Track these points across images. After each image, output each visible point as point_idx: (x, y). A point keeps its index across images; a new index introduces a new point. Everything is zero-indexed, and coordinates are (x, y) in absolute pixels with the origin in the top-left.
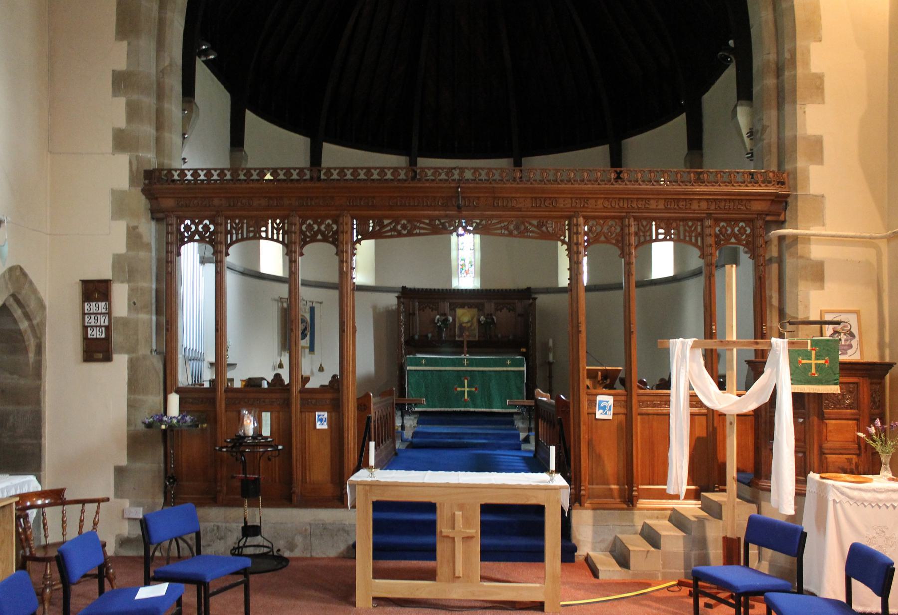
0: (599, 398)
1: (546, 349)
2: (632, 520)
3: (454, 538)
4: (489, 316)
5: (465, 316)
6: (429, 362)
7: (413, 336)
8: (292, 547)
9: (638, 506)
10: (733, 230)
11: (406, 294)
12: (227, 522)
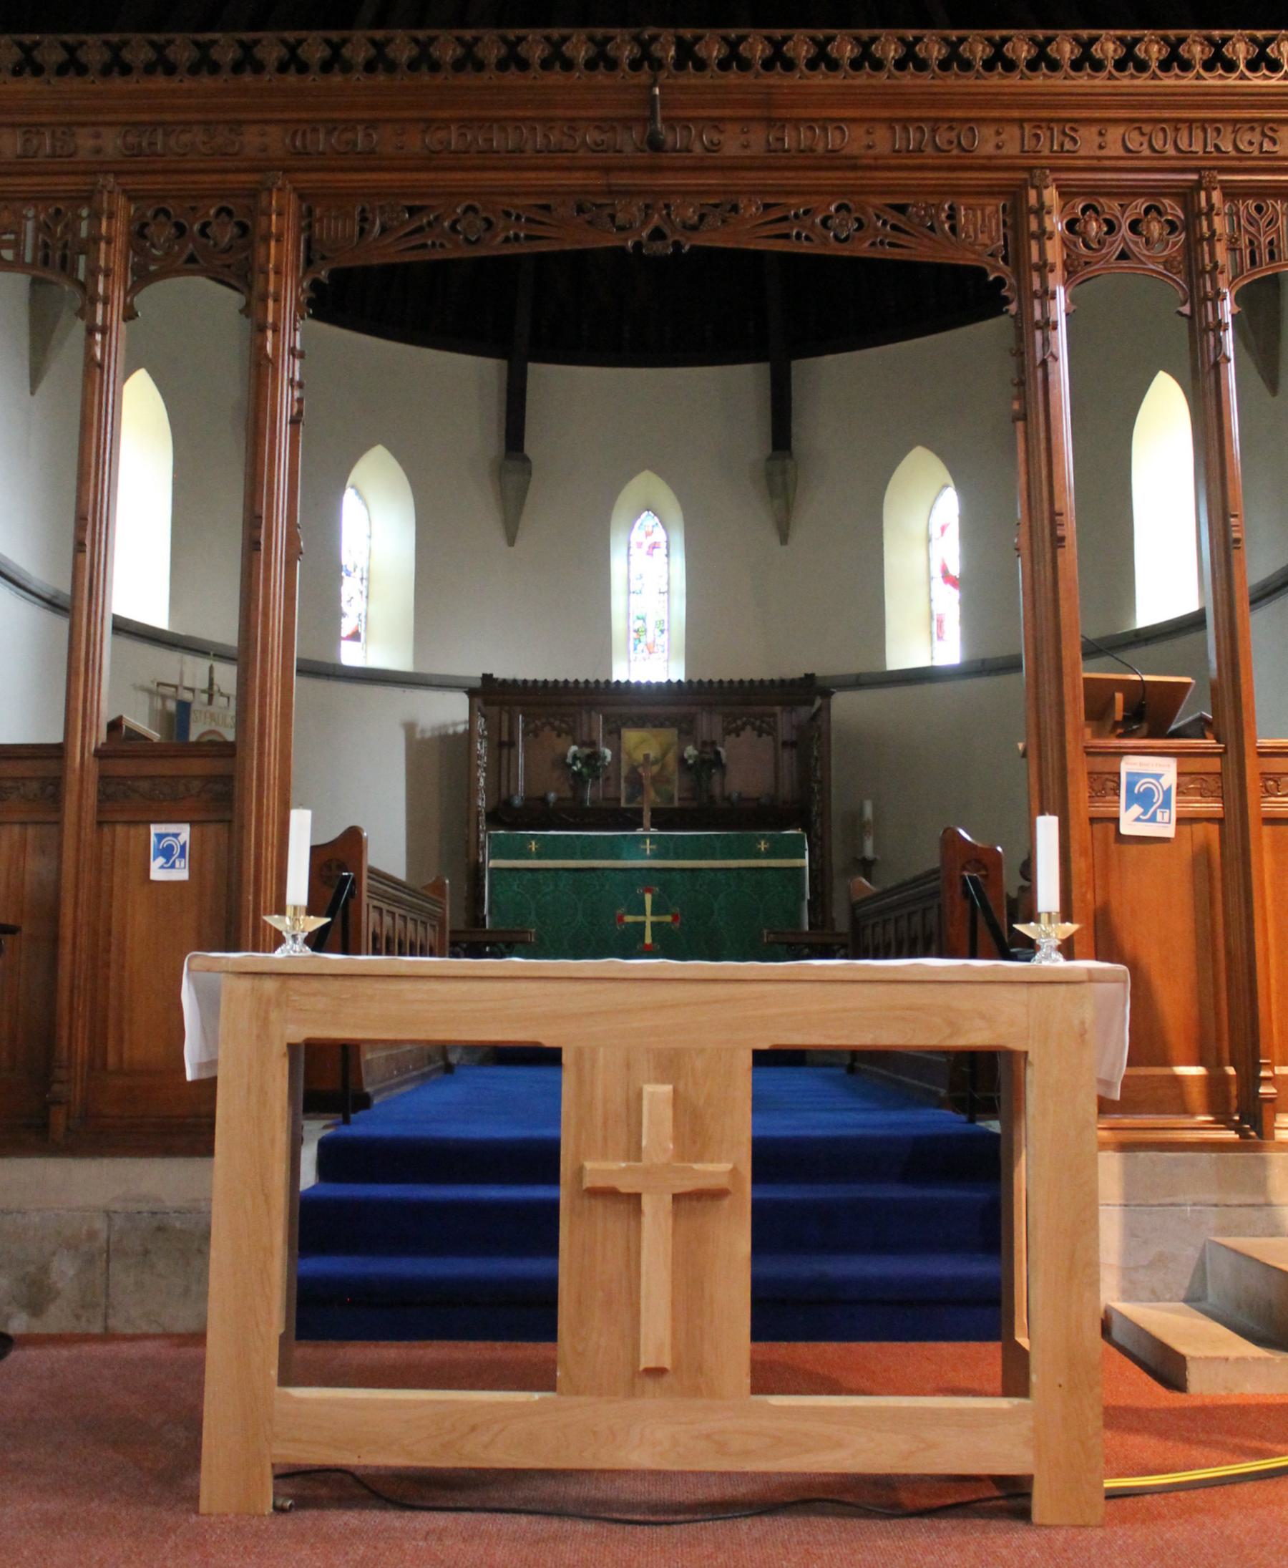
0: (1129, 765)
1: (856, 826)
2: (1261, 1185)
3: (636, 1198)
5: (641, 744)
7: (510, 798)
11: (489, 694)
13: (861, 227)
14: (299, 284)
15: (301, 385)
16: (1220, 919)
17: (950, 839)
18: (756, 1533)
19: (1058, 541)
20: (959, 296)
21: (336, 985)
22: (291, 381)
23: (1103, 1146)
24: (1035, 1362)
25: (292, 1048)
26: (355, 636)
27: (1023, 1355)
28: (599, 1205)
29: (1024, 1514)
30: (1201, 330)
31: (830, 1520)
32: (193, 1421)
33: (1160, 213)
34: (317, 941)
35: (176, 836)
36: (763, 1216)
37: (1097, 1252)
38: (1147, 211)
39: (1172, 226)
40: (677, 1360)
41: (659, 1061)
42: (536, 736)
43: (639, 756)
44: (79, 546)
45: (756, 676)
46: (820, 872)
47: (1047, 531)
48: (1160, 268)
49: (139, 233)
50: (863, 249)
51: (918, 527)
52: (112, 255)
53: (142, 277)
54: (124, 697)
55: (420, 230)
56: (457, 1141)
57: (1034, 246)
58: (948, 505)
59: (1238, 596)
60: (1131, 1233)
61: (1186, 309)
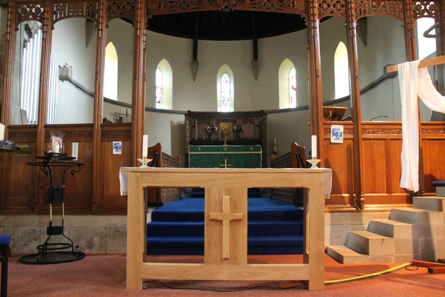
0: (333, 127)
1: (273, 144)
2: (361, 220)
3: (222, 221)
4: (239, 126)
5: (224, 126)
8: (90, 245)
9: (365, 209)
10: (425, 7)
11: (190, 115)
12: (41, 227)
13: (272, 5)
14: (145, 19)
15: (146, 42)
16: (353, 161)
17: (293, 145)
18: (248, 293)
19: (317, 76)
20: (294, 23)
21: (154, 174)
22: (143, 41)
23: (326, 212)
24: (310, 256)
25: (144, 188)
26: (159, 102)
27: (308, 255)
28: (213, 223)
29: (307, 288)
30: (349, 29)
31: (265, 290)
32: (125, 271)
33: (340, 3)
34: (150, 165)
35: (119, 144)
36: (249, 228)
37: (324, 232)
38: (337, 2)
39: (343, 6)
40: (231, 256)
41: (226, 191)
42: (200, 124)
43: (223, 129)
44: (96, 79)
45: (250, 111)
46: (264, 154)
47: (315, 74)
48: (340, 15)
49: (109, 8)
50: (273, 10)
51: (286, 77)
52: (103, 13)
53: (110, 18)
54: (106, 113)
55: (172, 6)
56: (182, 212)
57: (311, 10)
58: (293, 72)
59: (357, 93)
60: (332, 231)
61: (346, 24)
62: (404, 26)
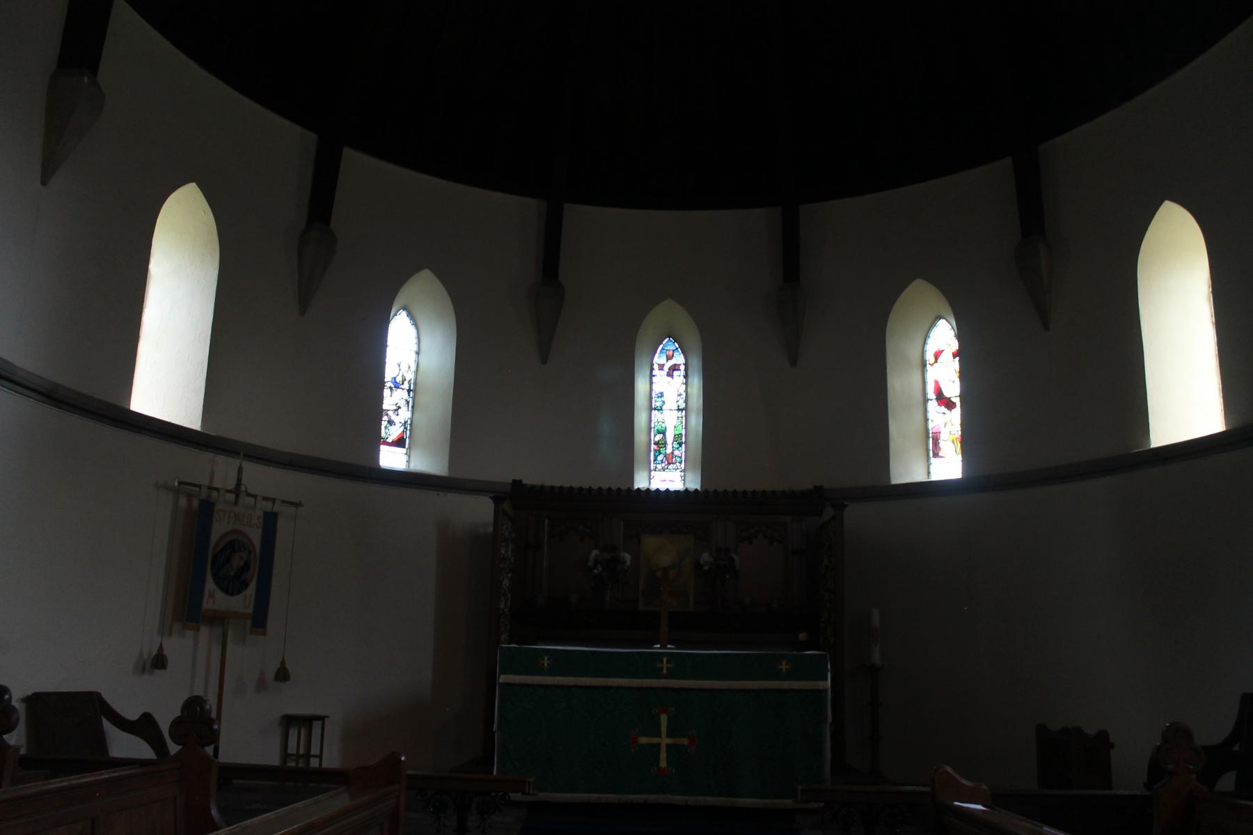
6: (563, 664)
11: (518, 500)
58: (944, 335)
62: (683, 406)
